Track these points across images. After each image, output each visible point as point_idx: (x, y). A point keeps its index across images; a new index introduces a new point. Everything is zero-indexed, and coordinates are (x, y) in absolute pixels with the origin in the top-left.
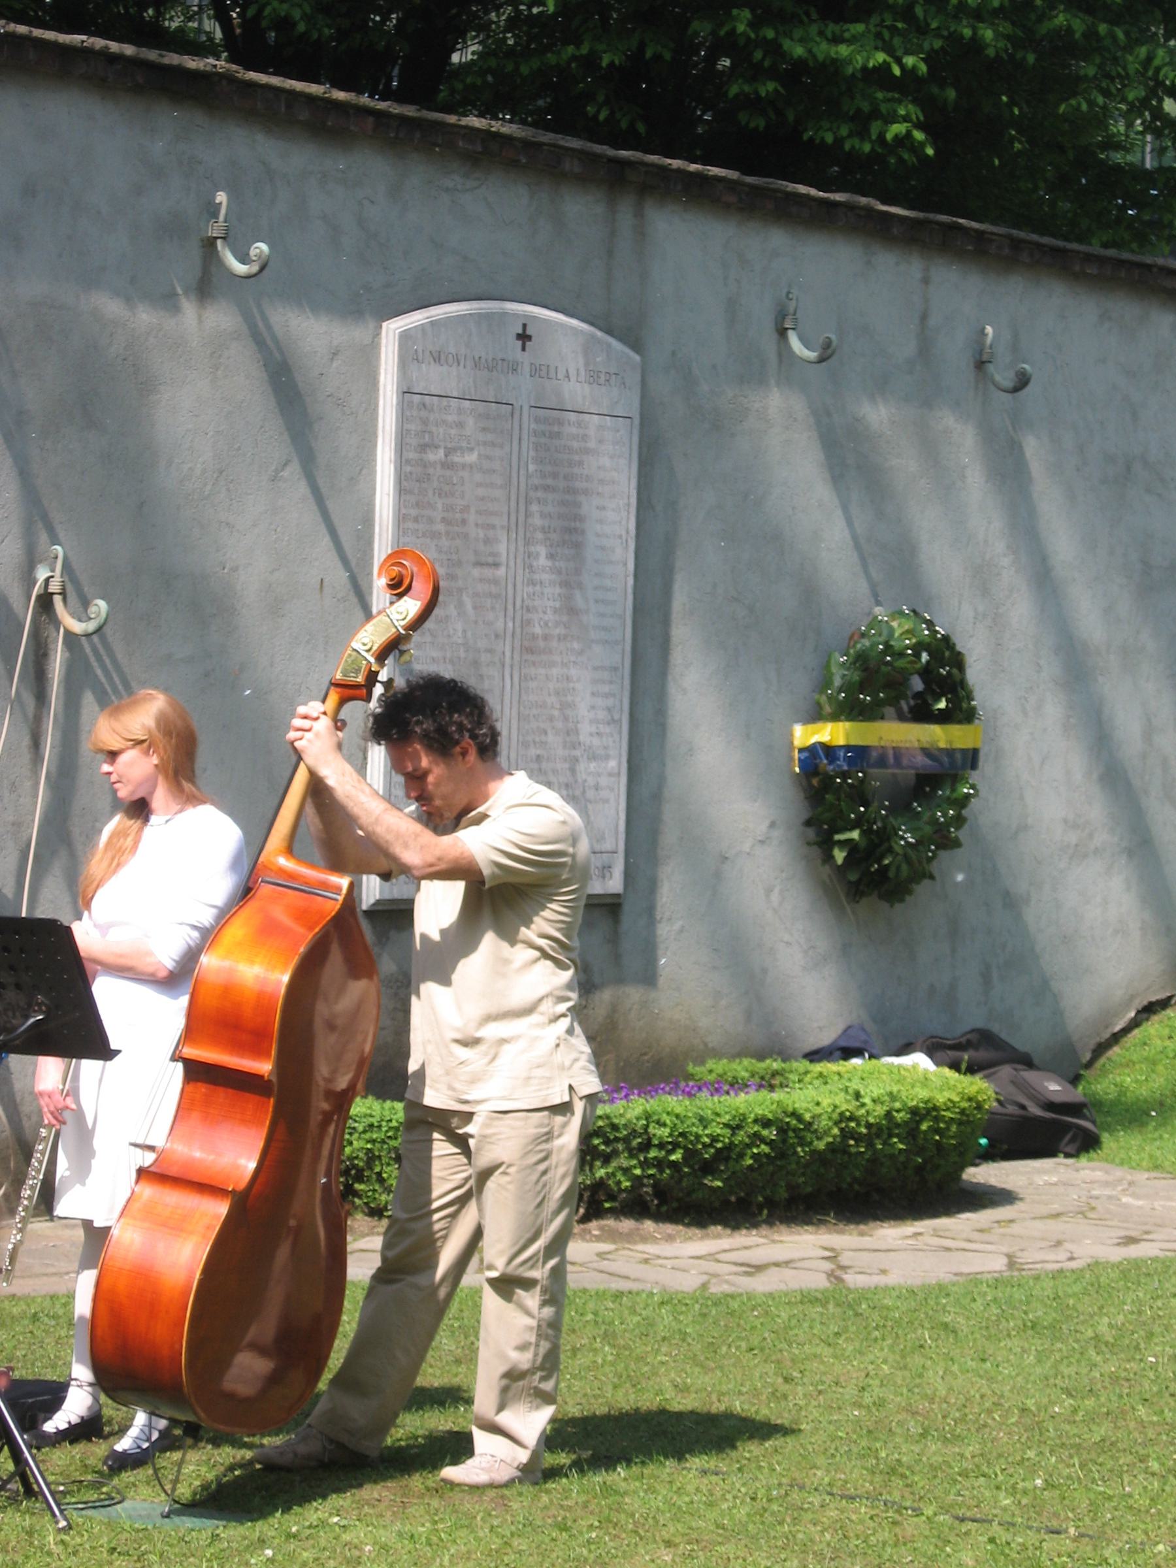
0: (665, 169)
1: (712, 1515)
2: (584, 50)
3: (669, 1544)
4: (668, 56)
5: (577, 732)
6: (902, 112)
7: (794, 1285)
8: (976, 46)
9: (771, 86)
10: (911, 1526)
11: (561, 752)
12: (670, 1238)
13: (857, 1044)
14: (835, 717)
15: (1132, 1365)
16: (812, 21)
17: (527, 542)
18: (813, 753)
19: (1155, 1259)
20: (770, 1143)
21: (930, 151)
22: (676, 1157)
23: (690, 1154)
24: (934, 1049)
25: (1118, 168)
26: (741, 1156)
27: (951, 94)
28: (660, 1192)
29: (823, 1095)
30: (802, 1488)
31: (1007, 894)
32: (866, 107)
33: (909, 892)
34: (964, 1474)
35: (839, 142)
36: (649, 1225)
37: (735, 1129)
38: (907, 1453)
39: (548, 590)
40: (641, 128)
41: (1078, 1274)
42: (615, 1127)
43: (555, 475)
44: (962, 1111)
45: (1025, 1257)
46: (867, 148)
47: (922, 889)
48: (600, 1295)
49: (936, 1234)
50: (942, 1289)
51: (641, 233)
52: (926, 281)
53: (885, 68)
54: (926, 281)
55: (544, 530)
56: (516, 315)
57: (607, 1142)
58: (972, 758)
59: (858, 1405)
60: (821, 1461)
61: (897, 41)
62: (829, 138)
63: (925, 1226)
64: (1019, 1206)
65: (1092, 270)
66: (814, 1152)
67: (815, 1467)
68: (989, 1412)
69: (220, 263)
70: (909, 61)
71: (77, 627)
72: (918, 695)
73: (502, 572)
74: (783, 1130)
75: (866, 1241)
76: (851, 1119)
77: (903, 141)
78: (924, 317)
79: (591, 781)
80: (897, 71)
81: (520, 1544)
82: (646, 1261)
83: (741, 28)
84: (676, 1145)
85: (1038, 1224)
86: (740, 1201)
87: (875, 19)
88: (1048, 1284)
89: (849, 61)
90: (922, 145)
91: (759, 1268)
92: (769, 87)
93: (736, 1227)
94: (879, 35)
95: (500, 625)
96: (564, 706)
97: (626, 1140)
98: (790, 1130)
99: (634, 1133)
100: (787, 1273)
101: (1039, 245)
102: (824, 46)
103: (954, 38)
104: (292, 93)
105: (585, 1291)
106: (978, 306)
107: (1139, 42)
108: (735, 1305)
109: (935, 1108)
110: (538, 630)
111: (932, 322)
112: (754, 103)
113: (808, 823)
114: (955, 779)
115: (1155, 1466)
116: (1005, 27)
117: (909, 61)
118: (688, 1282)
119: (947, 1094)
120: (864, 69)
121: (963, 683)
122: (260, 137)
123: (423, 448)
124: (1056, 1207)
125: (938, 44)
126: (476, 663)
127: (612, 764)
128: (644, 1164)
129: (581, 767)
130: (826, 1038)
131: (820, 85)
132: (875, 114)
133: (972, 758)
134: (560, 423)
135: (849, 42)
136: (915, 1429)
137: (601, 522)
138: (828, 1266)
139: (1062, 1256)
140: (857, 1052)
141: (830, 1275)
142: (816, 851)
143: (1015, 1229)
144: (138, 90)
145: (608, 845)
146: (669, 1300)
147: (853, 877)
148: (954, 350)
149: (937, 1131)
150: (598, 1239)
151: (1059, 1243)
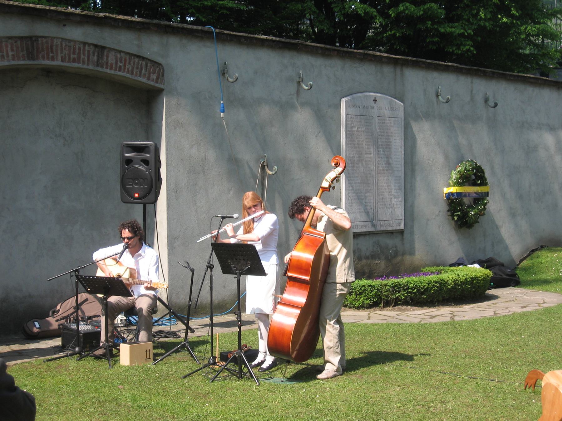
0: (407, 60)
1: (411, 379)
2: (393, 32)
3: (399, 386)
4: (412, 33)
5: (391, 192)
6: (468, 43)
7: (441, 321)
8: (485, 27)
9: (437, 39)
10: (458, 379)
11: (388, 197)
12: (414, 310)
13: (461, 262)
14: (454, 186)
15: (519, 338)
16: (445, 23)
17: (378, 148)
18: (449, 195)
19: (529, 312)
20: (437, 287)
21: (475, 52)
22: (415, 291)
23: (418, 290)
24: (481, 263)
25: (521, 54)
26: (431, 290)
27: (479, 39)
28: (412, 299)
29: (450, 275)
30: (433, 371)
31: (497, 226)
32: (459, 43)
33: (473, 226)
34: (473, 367)
35: (453, 51)
36: (409, 307)
37: (429, 284)
38: (461, 361)
39: (383, 159)
40: (407, 50)
41: (509, 316)
42: (400, 285)
43: (384, 132)
44: (484, 278)
45: (498, 312)
46: (460, 52)
47: (476, 225)
48: (395, 325)
49: (478, 307)
50: (476, 321)
51: (402, 75)
52: (472, 83)
53: (463, 33)
54: (472, 83)
55: (381, 145)
56: (373, 96)
57: (398, 288)
58: (487, 194)
59: (451, 350)
60: (440, 364)
61: (466, 27)
62: (451, 50)
63: (475, 305)
64: (499, 299)
65: (512, 78)
66: (448, 289)
67: (438, 366)
68: (482, 351)
69: (302, 87)
70: (469, 31)
71: (271, 173)
72: (473, 180)
73: (372, 155)
74: (440, 284)
75: (461, 309)
76: (457, 280)
77: (468, 50)
78: (472, 91)
79: (395, 203)
80: (466, 34)
81: (364, 387)
82: (408, 316)
83: (429, 26)
84: (415, 288)
85: (503, 304)
86: (431, 300)
87: (461, 22)
88: (502, 318)
89: (455, 32)
90: (473, 51)
91: (434, 317)
92: (436, 39)
93: (430, 307)
94: (462, 26)
95: (372, 168)
96: (388, 186)
97: (403, 287)
98: (442, 284)
99: (405, 286)
100: (441, 317)
101: (499, 73)
102: (449, 29)
103: (479, 25)
104: (317, 47)
105: (391, 324)
106: (482, 87)
107: (524, 24)
108: (426, 326)
109: (477, 277)
110: (381, 169)
111: (474, 92)
112: (433, 43)
113: (448, 211)
114: (483, 199)
115: (519, 363)
116: (491, 22)
117: (469, 31)
118: (417, 321)
119: (480, 274)
120: (458, 34)
121: (484, 177)
122: (310, 57)
123: (352, 127)
124: (507, 299)
125: (476, 27)
126: (366, 177)
127: (400, 199)
128: (407, 293)
129: (393, 200)
130: (454, 261)
131: (447, 38)
132: (461, 44)
133: (487, 194)
134: (384, 120)
135: (454, 28)
136: (463, 355)
137: (395, 143)
138: (451, 316)
139: (507, 311)
140: (462, 264)
141: (451, 318)
142: (450, 217)
143: (497, 305)
144: (280, 48)
145: (400, 218)
146: (412, 325)
147: (459, 223)
148: (479, 98)
149: (478, 283)
150: (397, 311)
151: (507, 308)
